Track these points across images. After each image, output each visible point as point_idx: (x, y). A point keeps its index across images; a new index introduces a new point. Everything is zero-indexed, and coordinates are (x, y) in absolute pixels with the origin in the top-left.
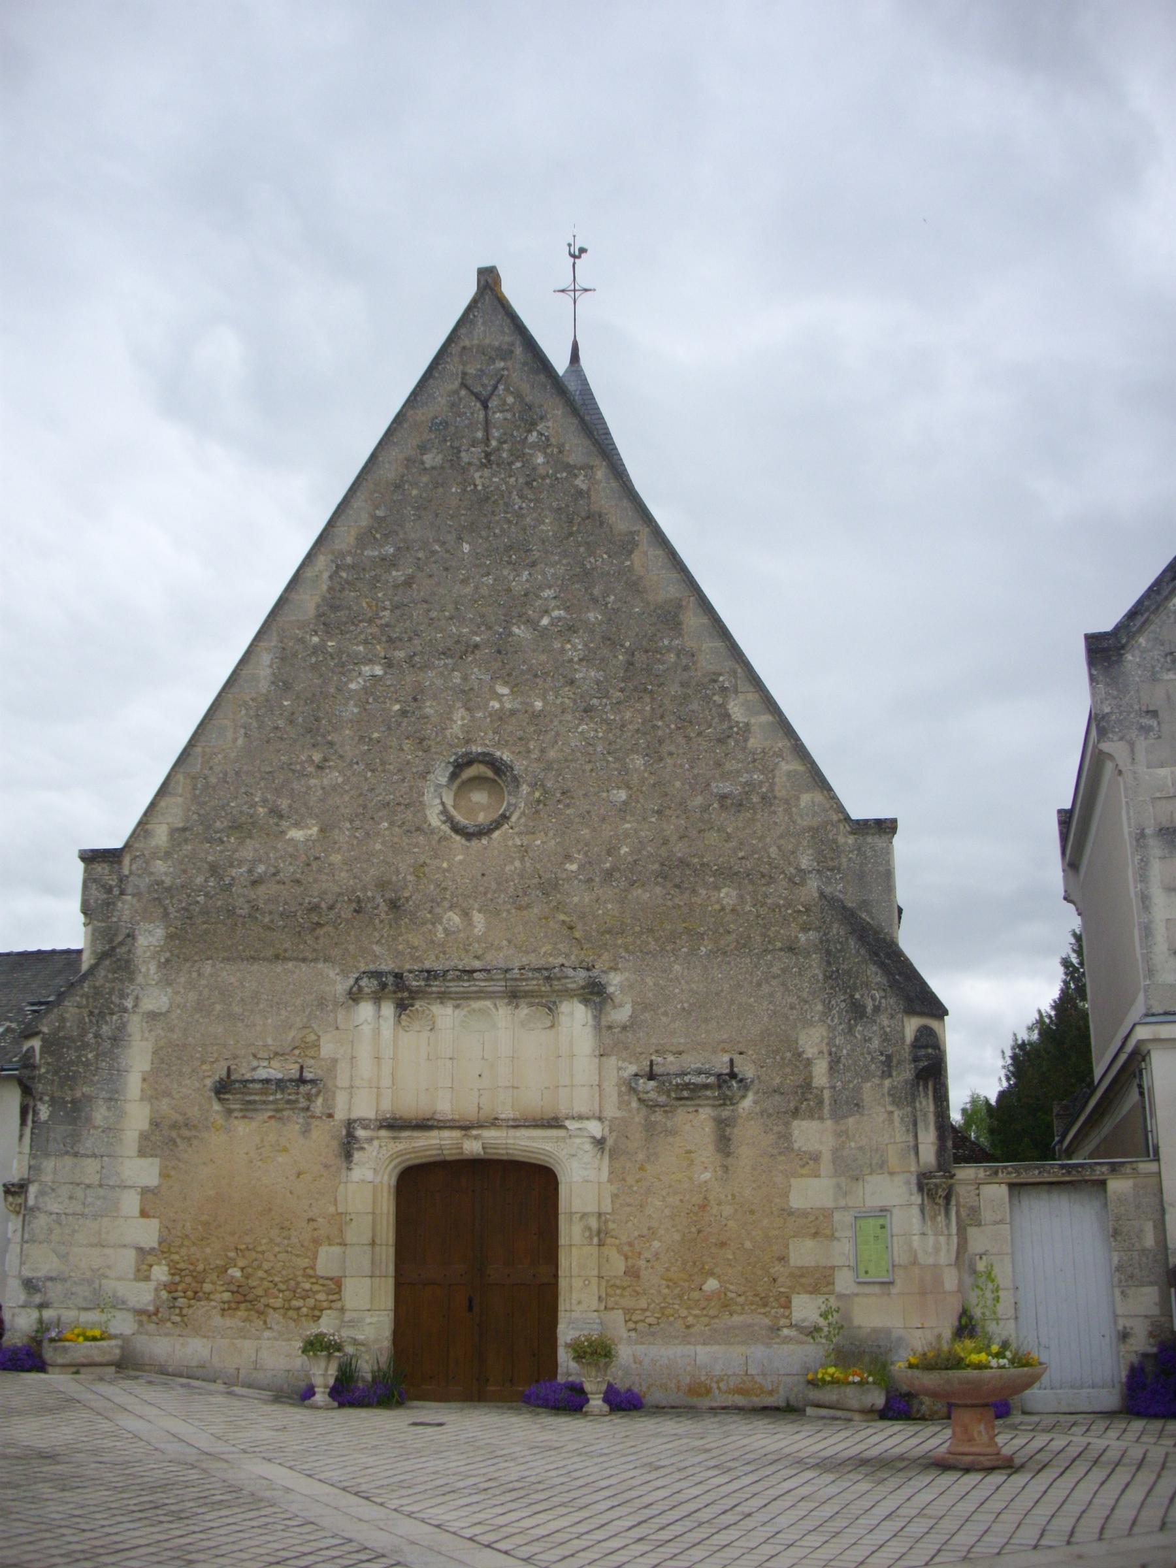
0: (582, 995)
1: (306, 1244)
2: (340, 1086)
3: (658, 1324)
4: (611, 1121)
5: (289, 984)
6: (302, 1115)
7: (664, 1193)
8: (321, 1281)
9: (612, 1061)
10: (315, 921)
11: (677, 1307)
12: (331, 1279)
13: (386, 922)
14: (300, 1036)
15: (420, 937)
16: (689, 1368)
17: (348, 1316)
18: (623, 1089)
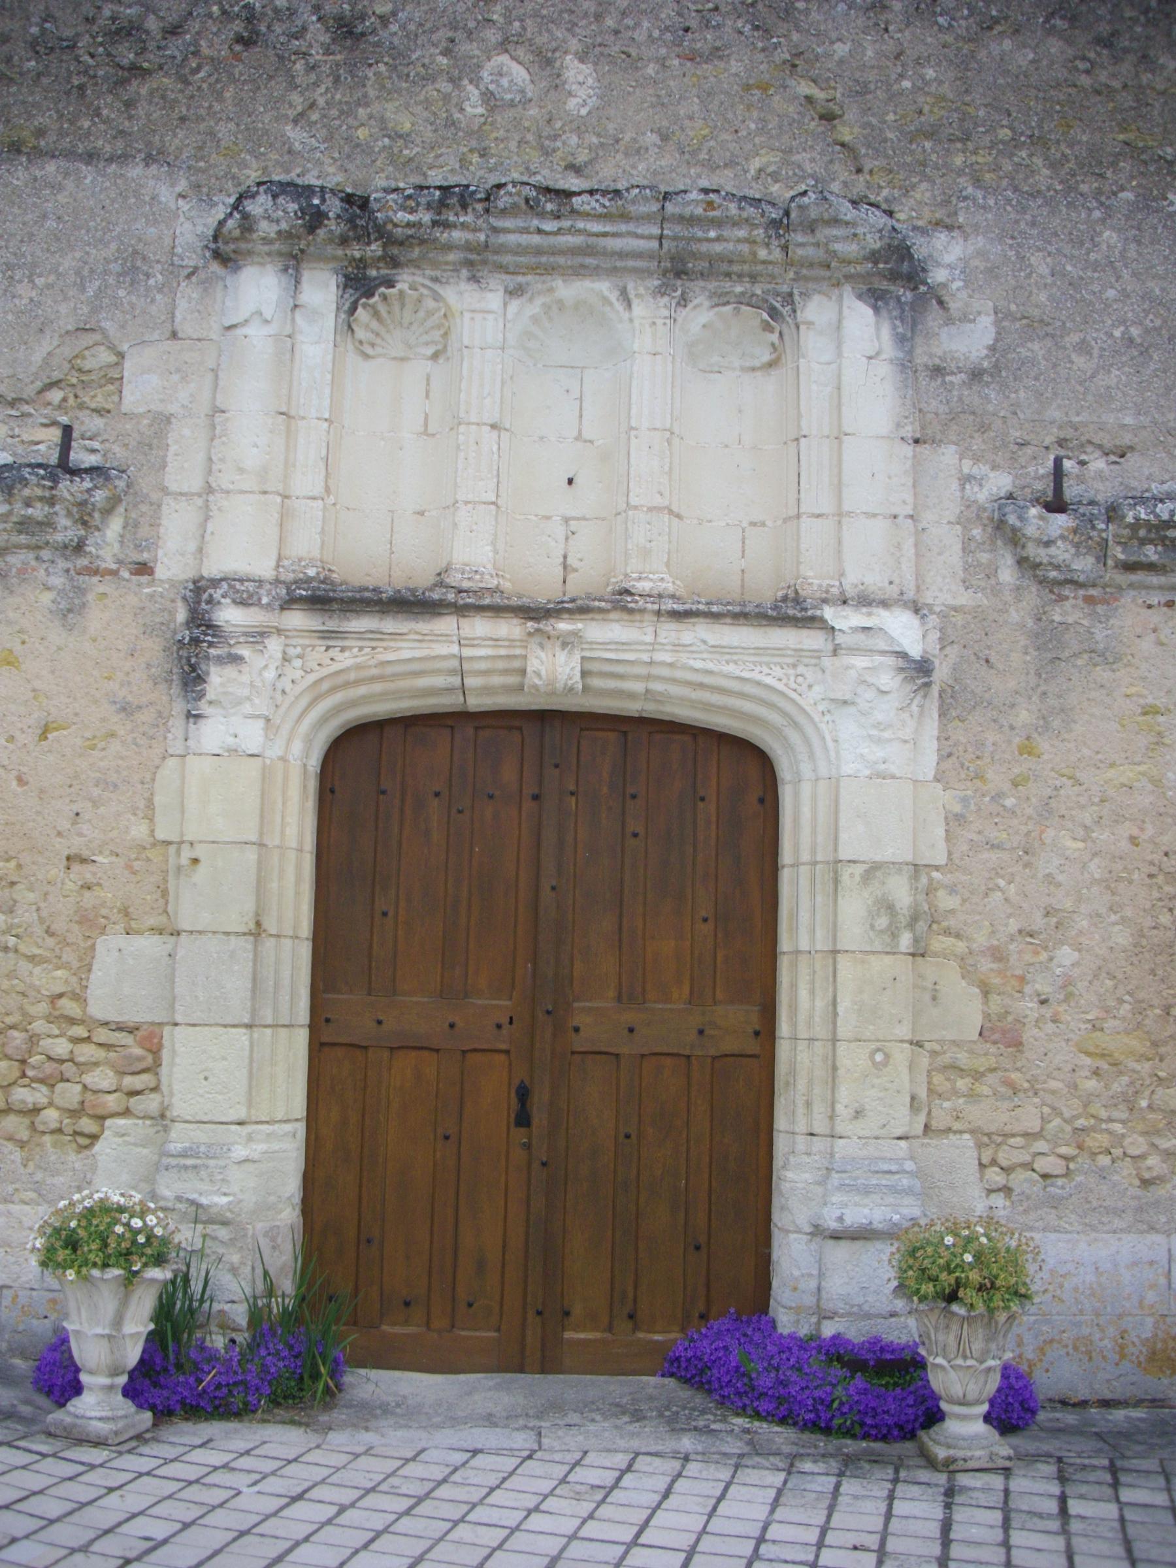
0: (865, 277)
1: (59, 926)
2: (173, 487)
3: (1068, 1174)
4: (943, 616)
5: (44, 217)
6: (62, 564)
7: (1087, 817)
8: (102, 1035)
9: (948, 455)
10: (125, 62)
11: (1118, 1127)
12: (132, 1030)
13: (326, 69)
14: (68, 352)
15: (418, 109)
16: (1151, 1297)
17: (179, 1138)
18: (977, 532)
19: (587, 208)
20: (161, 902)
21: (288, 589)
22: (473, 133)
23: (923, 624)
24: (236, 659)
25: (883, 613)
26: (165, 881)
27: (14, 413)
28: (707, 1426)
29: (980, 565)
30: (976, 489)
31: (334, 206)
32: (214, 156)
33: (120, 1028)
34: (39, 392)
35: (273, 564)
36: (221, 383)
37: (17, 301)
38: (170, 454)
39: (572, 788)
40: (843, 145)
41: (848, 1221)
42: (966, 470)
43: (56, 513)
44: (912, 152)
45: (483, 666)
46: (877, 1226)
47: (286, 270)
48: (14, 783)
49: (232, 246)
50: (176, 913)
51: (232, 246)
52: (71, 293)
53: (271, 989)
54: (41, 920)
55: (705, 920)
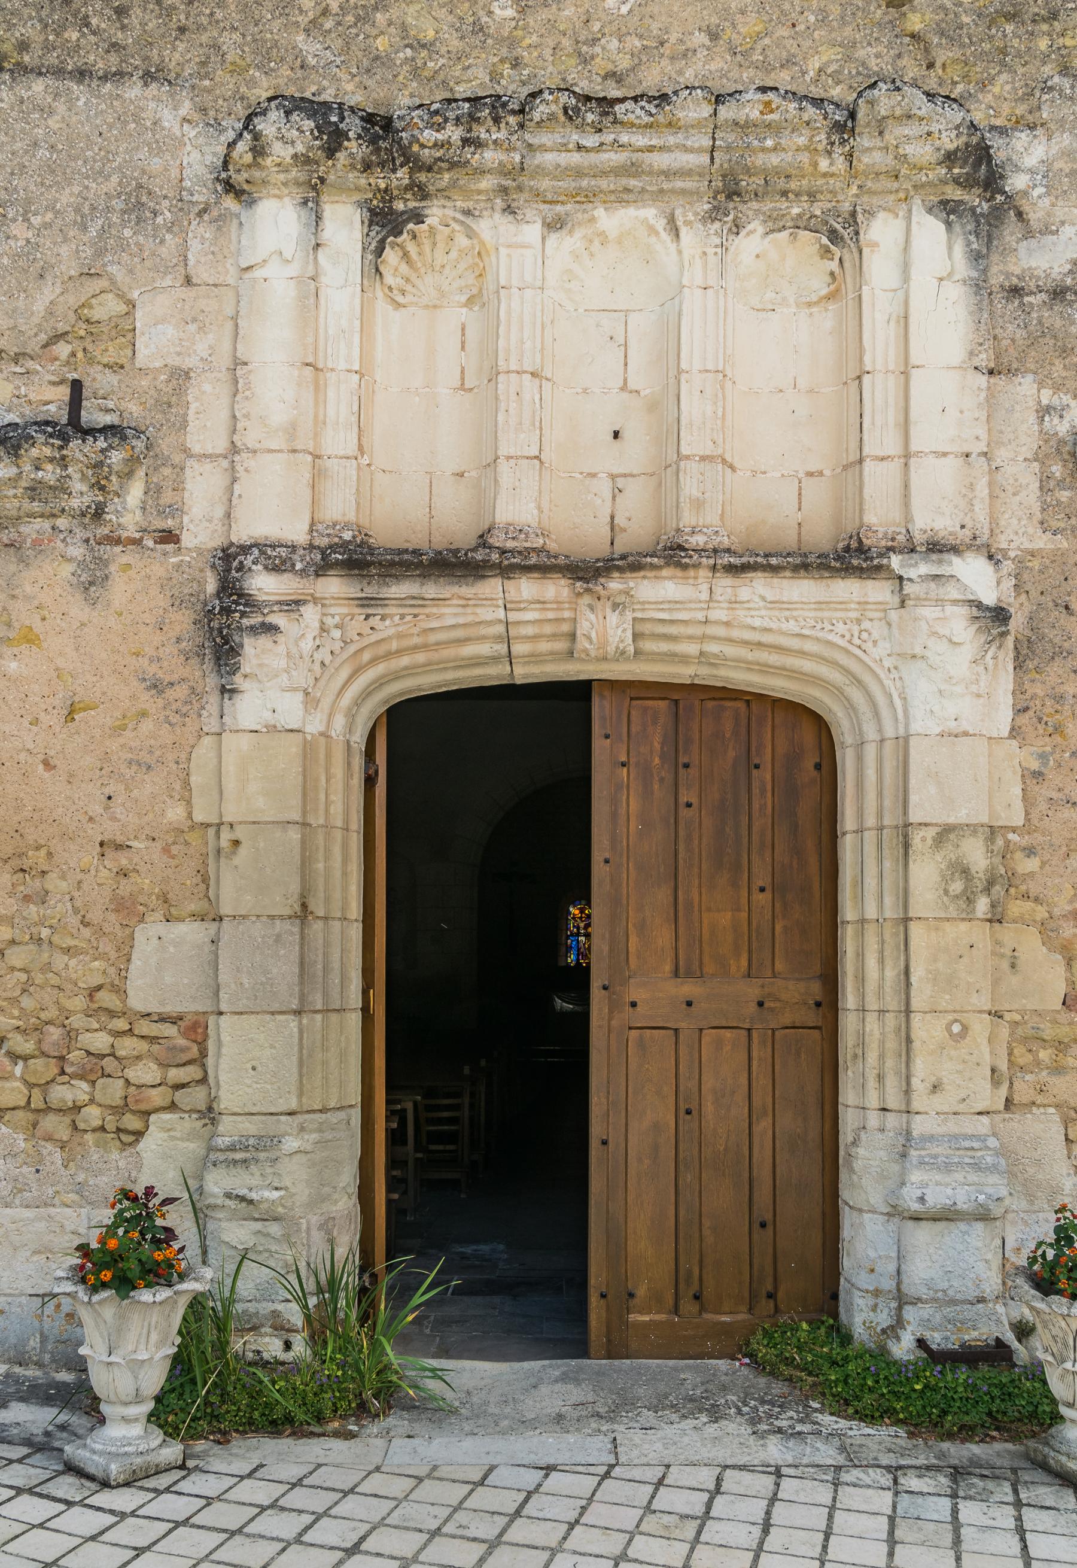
1: (95, 916)
2: (197, 449)
8: (145, 1027)
9: (1025, 387)
12: (174, 1020)
14: (72, 300)
17: (229, 1130)
18: (1057, 470)
19: (631, 116)
20: (203, 886)
21: (323, 553)
22: (503, 40)
23: (997, 571)
24: (270, 629)
25: (955, 560)
26: (205, 864)
27: (18, 370)
28: (792, 1427)
29: (1059, 503)
30: (1056, 420)
31: (353, 125)
32: (220, 72)
33: (163, 1019)
34: (44, 346)
35: (306, 527)
36: (241, 332)
37: (11, 242)
38: (191, 412)
39: (624, 759)
40: (913, 36)
41: (930, 1200)
42: (1045, 402)
43: (68, 476)
44: (991, 38)
45: (529, 630)
46: (961, 1206)
47: (305, 203)
48: (41, 767)
49: (245, 175)
50: (218, 897)
51: (245, 175)
52: (71, 234)
53: (320, 973)
54: (76, 910)
55: (762, 890)
